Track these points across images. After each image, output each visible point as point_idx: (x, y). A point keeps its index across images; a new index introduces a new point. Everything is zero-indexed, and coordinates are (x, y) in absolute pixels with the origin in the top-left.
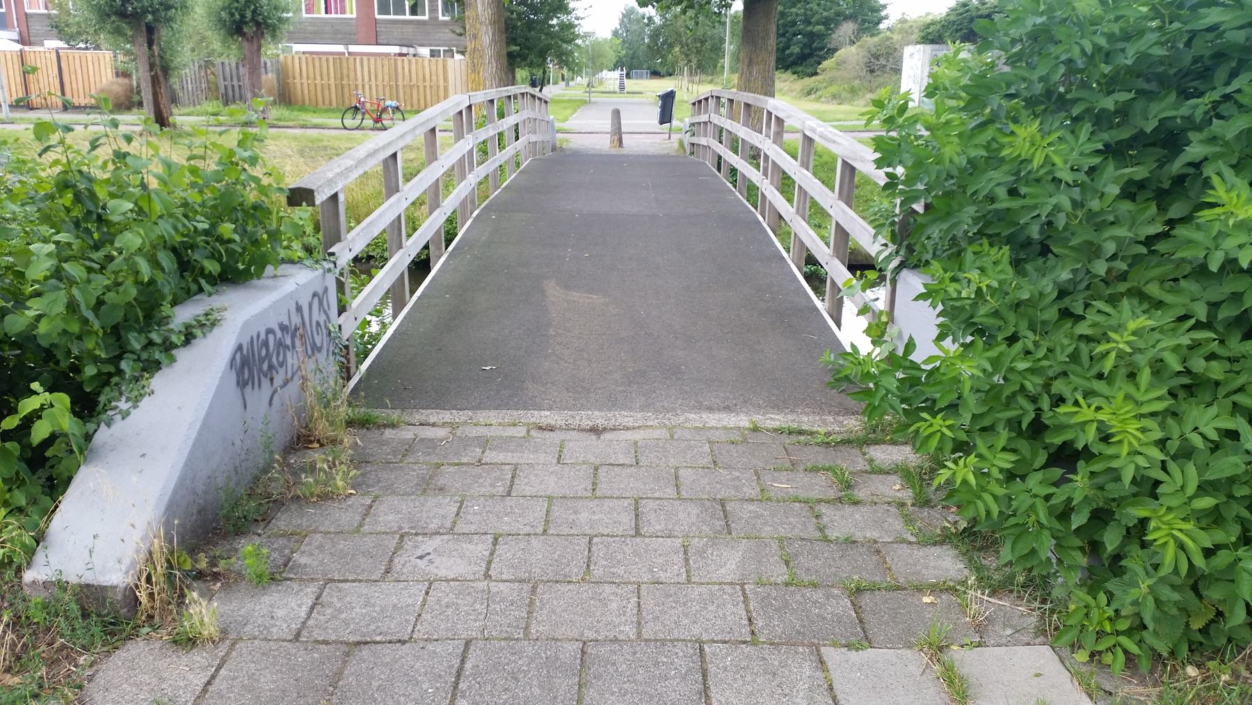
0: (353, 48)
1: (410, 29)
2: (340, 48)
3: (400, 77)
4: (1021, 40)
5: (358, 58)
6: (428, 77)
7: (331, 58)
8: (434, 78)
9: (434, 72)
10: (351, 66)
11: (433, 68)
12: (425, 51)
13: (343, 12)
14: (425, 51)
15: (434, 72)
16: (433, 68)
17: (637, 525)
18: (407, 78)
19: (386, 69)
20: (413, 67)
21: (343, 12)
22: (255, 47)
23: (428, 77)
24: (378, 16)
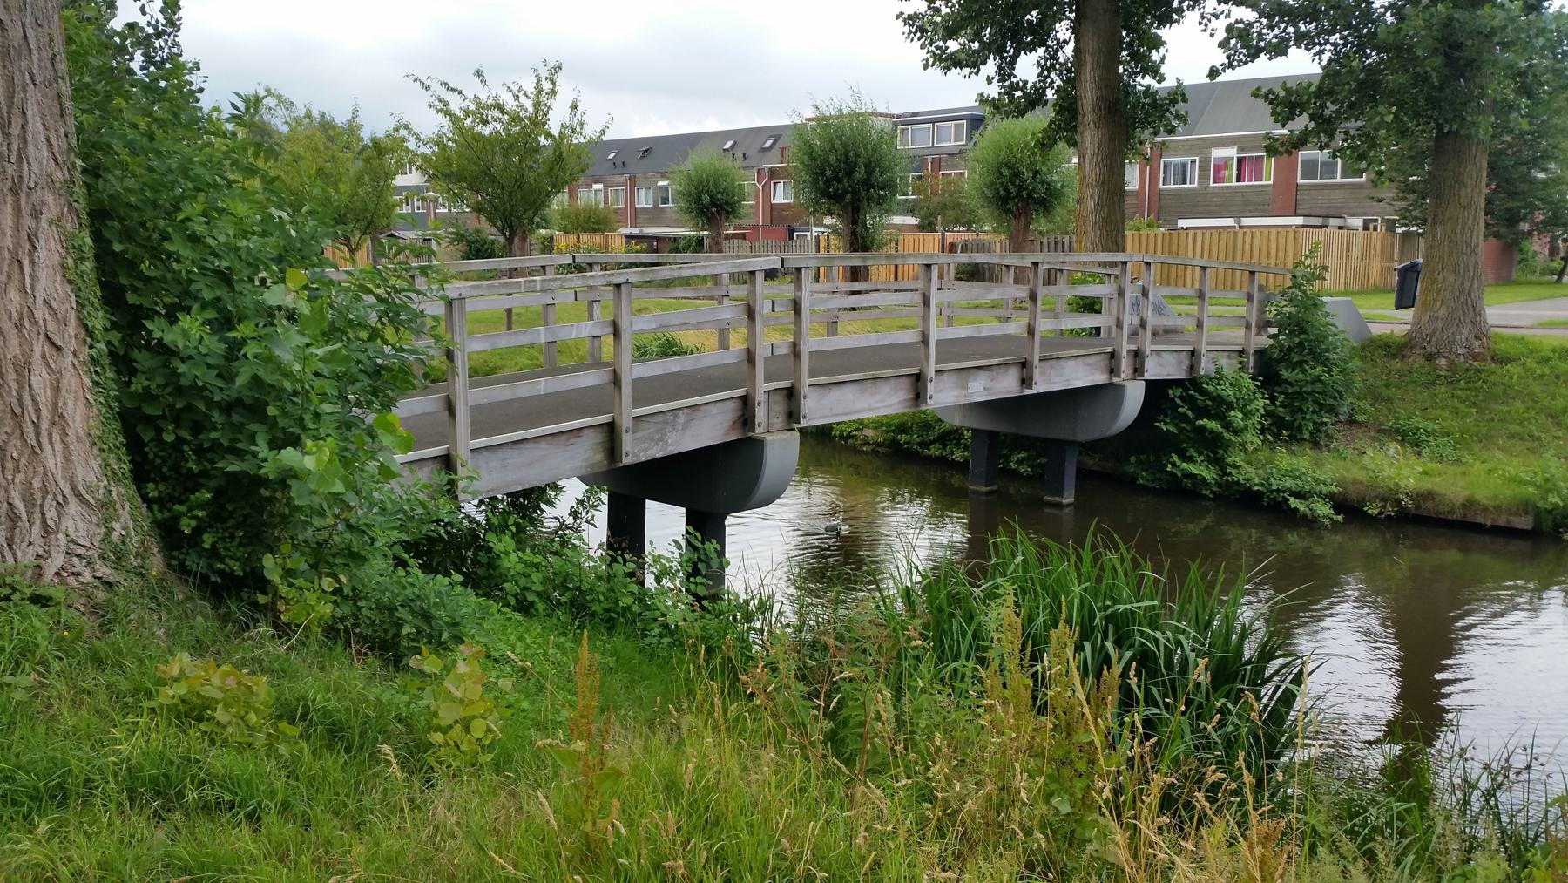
0: (1247, 221)
1: (1340, 194)
2: (1230, 222)
3: (1239, 253)
4: (411, 732)
5: (1199, 233)
6: (1273, 252)
7: (1274, 231)
8: (1281, 254)
9: (1282, 247)
10: (1182, 243)
11: (1282, 241)
12: (1357, 222)
13: (1184, 182)
14: (1357, 222)
15: (1282, 247)
16: (1282, 241)
17: (1479, 528)
18: (1247, 254)
19: (1223, 243)
20: (1256, 241)
21: (1184, 182)
22: (1022, 224)
23: (1273, 252)
24: (1300, 181)
